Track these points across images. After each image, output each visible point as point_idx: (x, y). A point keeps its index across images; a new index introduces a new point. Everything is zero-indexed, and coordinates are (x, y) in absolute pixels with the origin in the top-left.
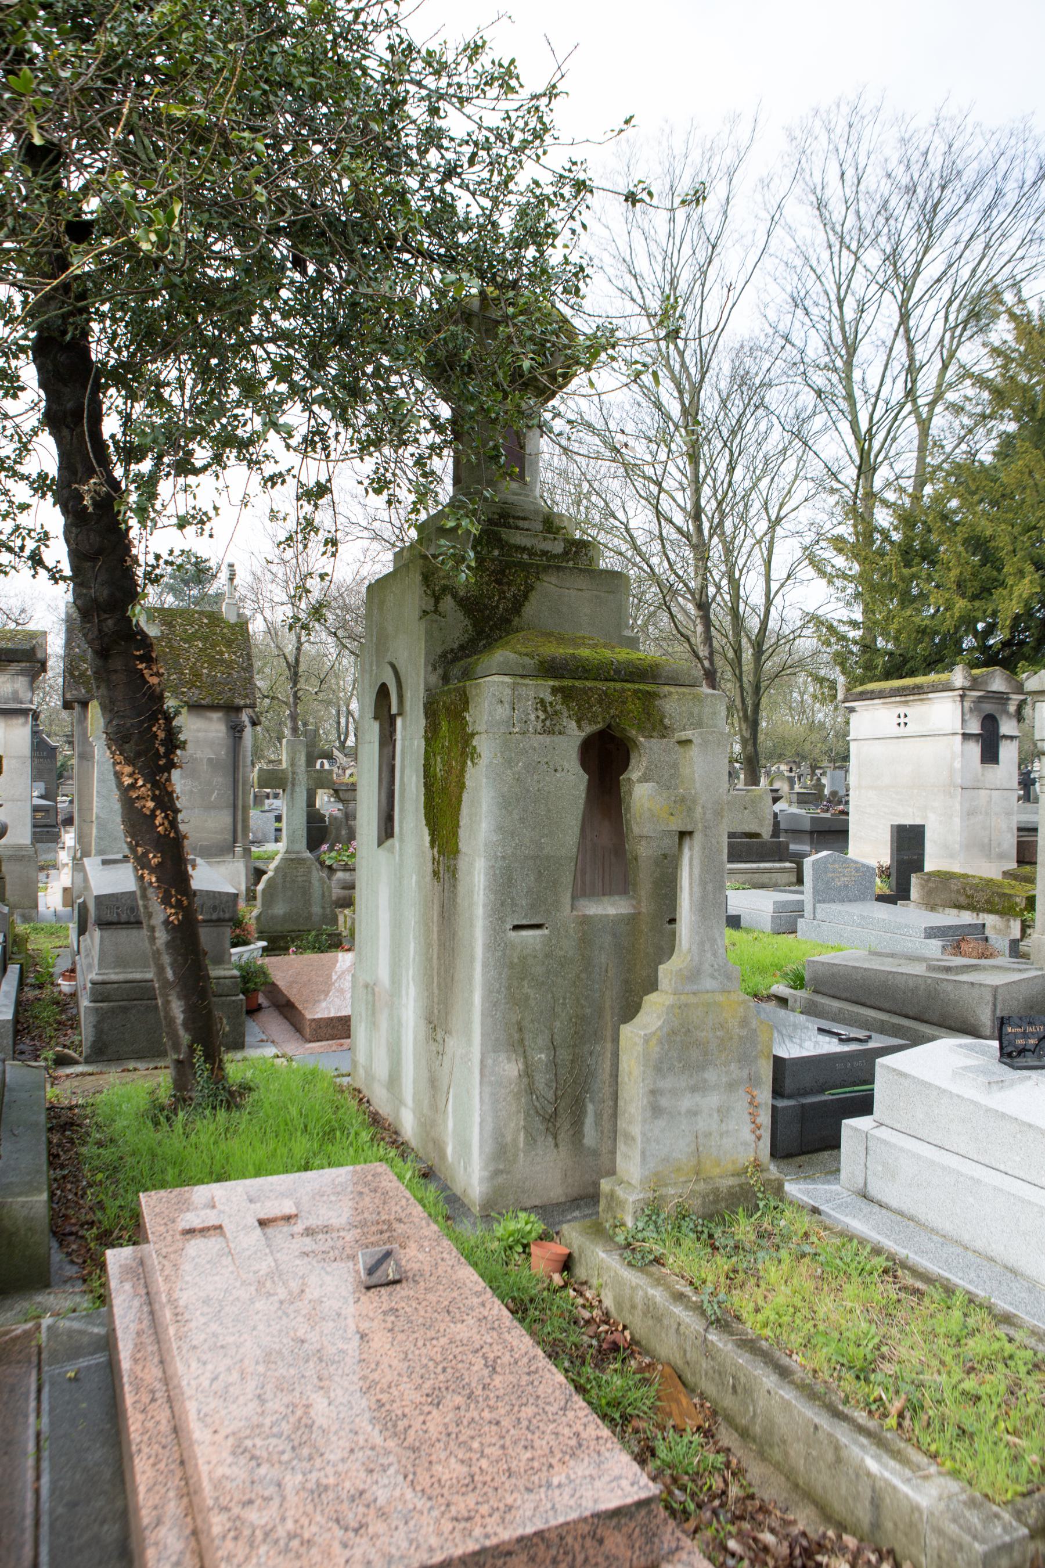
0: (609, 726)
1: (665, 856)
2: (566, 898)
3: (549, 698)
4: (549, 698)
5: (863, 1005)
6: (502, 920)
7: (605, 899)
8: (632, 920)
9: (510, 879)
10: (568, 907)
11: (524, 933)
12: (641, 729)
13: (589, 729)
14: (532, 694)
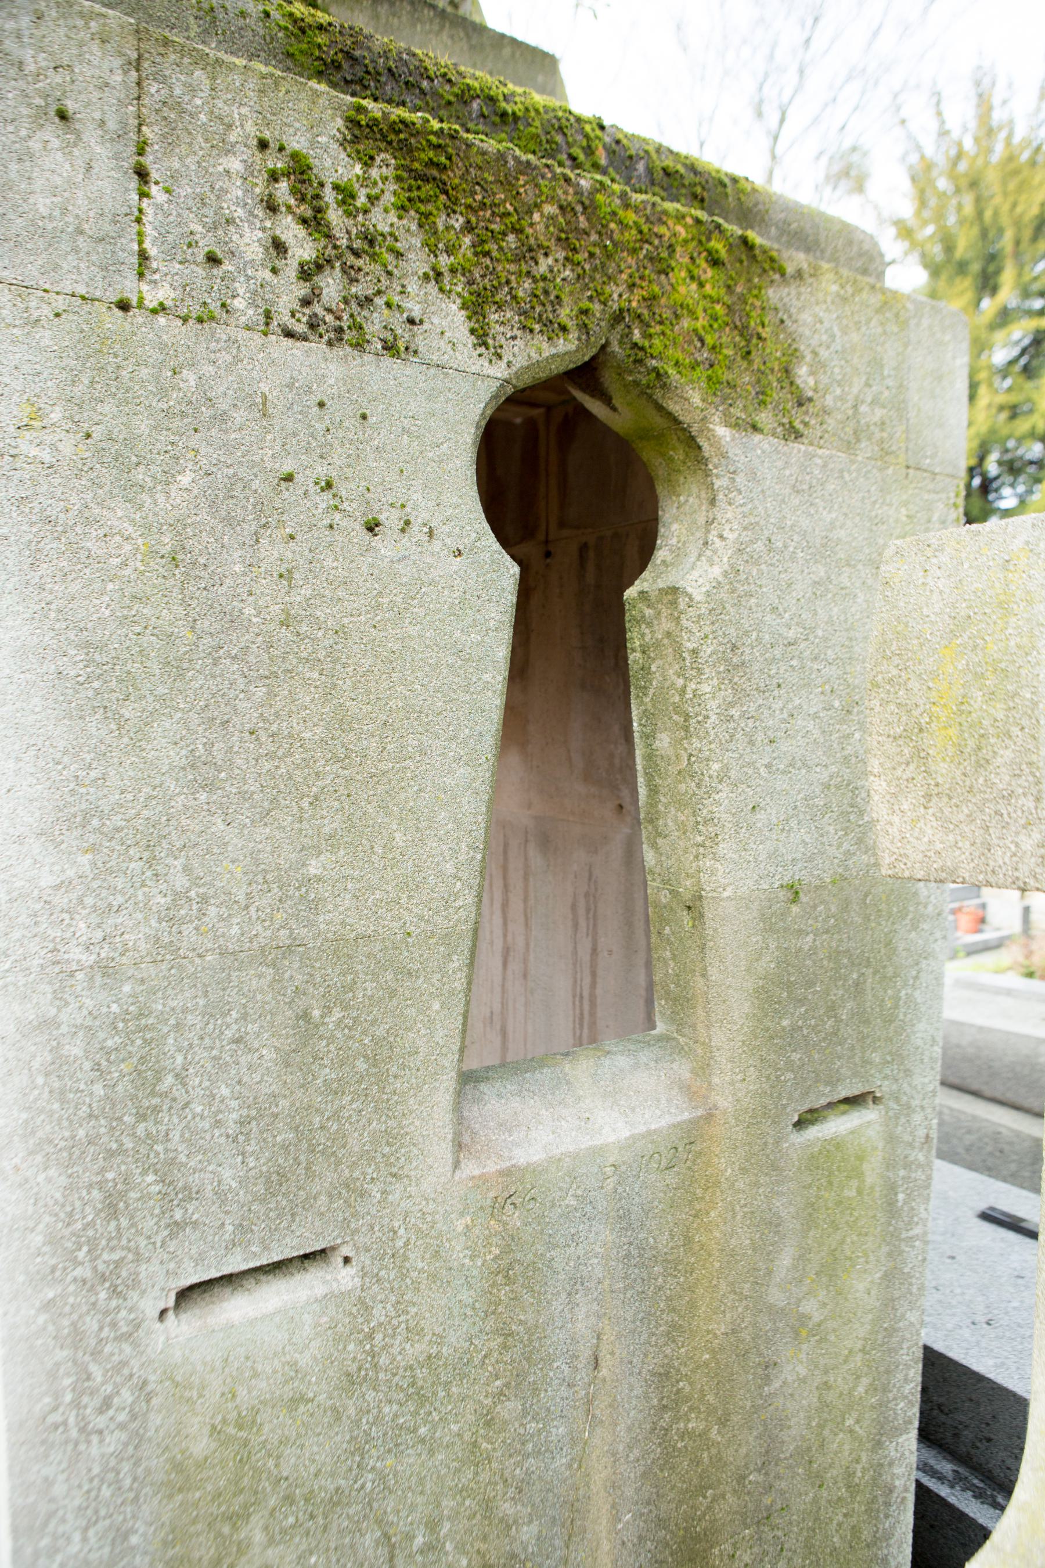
0: (587, 374)
1: (794, 892)
2: (430, 1111)
3: (336, 166)
4: (336, 166)
5: (976, 1094)
6: (116, 1283)
7: (582, 1069)
8: (687, 1147)
9: (147, 1075)
10: (444, 1151)
11: (236, 1309)
12: (721, 390)
13: (530, 354)
14: (247, 128)
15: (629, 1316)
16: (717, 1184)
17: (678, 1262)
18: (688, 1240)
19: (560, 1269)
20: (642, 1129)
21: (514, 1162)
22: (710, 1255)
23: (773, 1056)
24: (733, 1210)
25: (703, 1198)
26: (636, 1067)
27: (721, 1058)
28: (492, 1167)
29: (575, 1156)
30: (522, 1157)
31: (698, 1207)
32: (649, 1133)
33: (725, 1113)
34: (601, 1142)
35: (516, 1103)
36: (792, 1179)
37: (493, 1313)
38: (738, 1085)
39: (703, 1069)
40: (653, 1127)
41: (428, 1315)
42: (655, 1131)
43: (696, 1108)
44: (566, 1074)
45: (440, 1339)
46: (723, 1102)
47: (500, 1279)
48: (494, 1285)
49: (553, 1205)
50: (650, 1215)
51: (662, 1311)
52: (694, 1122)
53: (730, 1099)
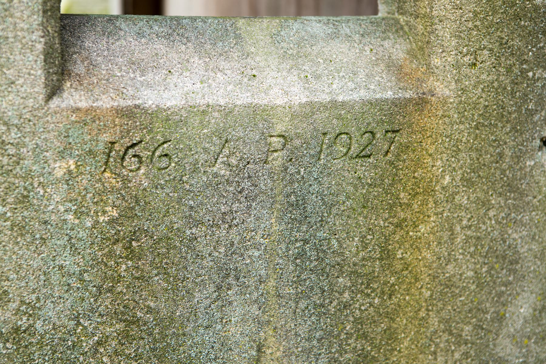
8: (388, 130)
15: (303, 331)
16: (429, 191)
17: (371, 278)
18: (387, 255)
19: (206, 253)
20: (325, 98)
21: (137, 102)
22: (417, 280)
23: (517, 42)
24: (451, 229)
25: (409, 205)
26: (334, 36)
27: (445, 32)
28: (106, 102)
29: (227, 112)
30: (150, 99)
31: (402, 215)
32: (334, 104)
33: (444, 102)
34: (265, 102)
35: (160, 46)
36: (535, 209)
37: (110, 290)
38: (465, 70)
39: (422, 50)
40: (340, 98)
41: (13, 276)
42: (343, 104)
43: (405, 89)
44: (237, 29)
45: (32, 310)
46: (443, 88)
47: (118, 249)
48: (110, 254)
49: (195, 170)
50: (334, 211)
51: (349, 335)
52: (400, 105)
53: (453, 86)
